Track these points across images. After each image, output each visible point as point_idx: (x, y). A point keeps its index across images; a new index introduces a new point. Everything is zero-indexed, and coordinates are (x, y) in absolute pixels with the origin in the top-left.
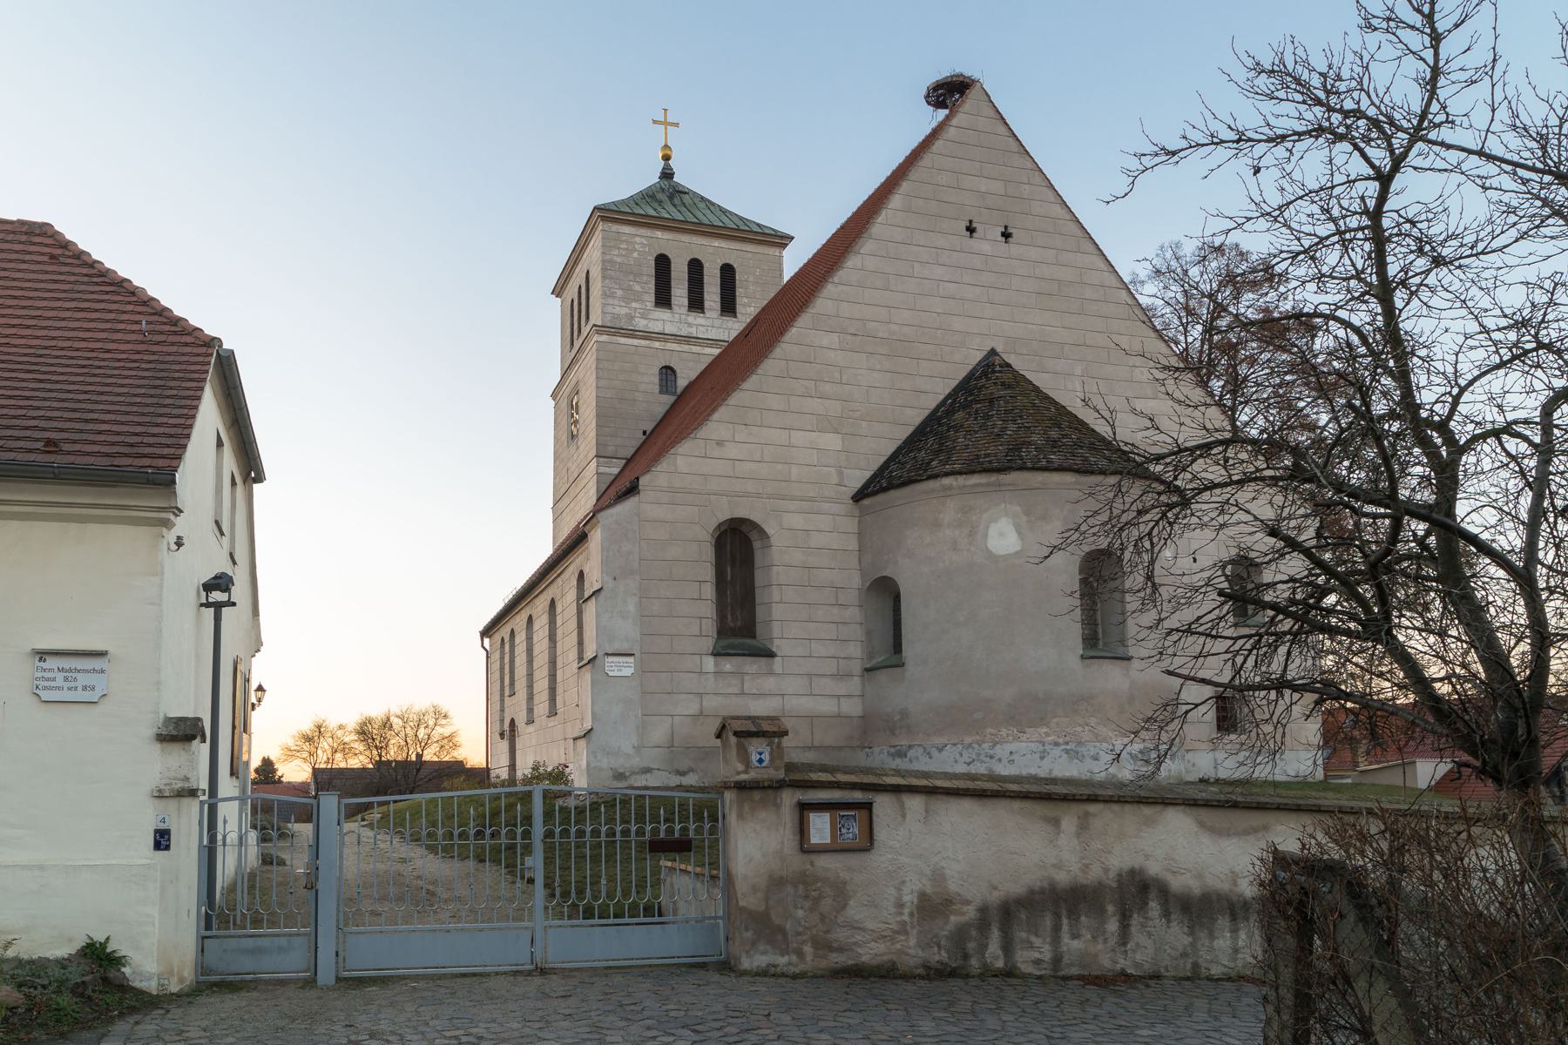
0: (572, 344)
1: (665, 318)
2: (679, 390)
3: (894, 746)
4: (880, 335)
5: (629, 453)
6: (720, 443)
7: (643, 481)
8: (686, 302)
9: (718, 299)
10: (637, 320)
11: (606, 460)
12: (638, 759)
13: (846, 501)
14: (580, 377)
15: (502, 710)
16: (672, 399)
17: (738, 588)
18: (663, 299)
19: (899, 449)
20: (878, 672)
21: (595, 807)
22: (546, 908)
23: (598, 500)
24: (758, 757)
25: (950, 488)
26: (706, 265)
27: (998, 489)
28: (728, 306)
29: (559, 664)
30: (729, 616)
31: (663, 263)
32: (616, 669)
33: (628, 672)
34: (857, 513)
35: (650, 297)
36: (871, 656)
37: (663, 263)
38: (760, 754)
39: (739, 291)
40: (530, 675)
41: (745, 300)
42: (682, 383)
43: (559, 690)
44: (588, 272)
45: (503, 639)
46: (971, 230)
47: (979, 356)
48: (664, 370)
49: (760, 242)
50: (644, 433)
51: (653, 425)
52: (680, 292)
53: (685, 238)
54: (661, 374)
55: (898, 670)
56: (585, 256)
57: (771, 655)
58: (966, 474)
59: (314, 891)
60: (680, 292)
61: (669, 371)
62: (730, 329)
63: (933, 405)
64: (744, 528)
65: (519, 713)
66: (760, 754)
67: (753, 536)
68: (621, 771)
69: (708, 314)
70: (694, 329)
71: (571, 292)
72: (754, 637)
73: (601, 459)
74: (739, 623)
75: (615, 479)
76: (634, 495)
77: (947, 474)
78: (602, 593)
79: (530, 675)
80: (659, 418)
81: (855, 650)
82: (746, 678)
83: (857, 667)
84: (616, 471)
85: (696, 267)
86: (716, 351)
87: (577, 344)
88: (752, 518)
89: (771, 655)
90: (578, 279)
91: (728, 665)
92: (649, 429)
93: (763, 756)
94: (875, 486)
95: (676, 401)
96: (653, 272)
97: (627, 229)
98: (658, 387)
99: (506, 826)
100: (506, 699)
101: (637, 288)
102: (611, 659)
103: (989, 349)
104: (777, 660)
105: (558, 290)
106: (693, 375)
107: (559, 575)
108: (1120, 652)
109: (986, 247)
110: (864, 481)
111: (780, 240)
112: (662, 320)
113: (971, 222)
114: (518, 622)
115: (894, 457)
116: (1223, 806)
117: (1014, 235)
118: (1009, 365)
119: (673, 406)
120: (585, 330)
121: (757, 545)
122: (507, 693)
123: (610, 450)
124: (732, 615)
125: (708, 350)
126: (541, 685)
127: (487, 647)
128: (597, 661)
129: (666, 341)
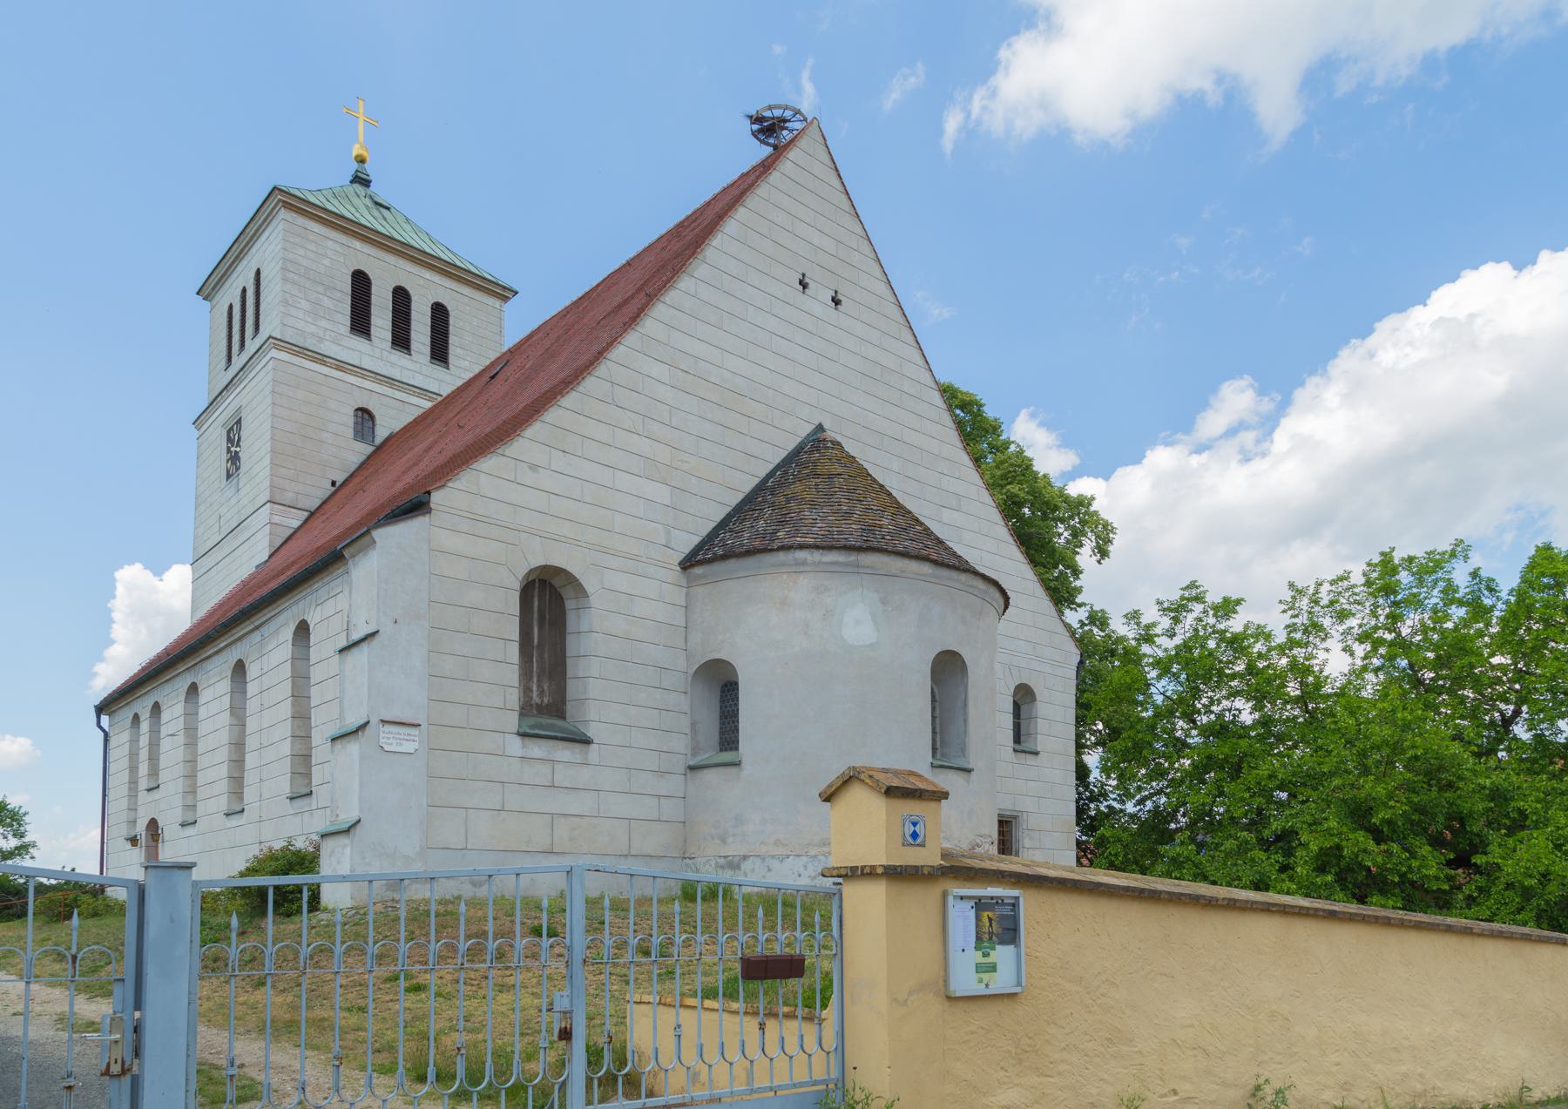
3: (725, 857)
4: (713, 380)
5: (314, 504)
6: (534, 467)
7: (437, 498)
8: (389, 336)
9: (428, 341)
10: (327, 343)
13: (673, 567)
14: (244, 403)
15: (133, 809)
16: (369, 449)
17: (546, 656)
18: (360, 323)
19: (728, 518)
20: (706, 771)
21: (388, 920)
22: (589, 1081)
23: (270, 557)
24: (912, 828)
25: (804, 563)
26: (414, 298)
27: (856, 570)
28: (440, 352)
29: (251, 743)
30: (535, 688)
31: (361, 283)
32: (394, 742)
33: (409, 747)
34: (684, 583)
35: (345, 319)
36: (695, 750)
37: (361, 283)
38: (915, 824)
39: (453, 340)
40: (192, 762)
42: (382, 433)
43: (250, 778)
44: (258, 273)
45: (136, 718)
46: (804, 285)
47: (809, 428)
48: (360, 413)
49: (479, 288)
50: (333, 483)
51: (346, 475)
52: (382, 319)
54: (356, 416)
55: (733, 770)
56: (253, 250)
57: (586, 741)
58: (823, 548)
59: (127, 1080)
60: (382, 319)
61: (366, 416)
62: (445, 382)
63: (763, 474)
64: (557, 582)
65: (166, 806)
66: (915, 824)
67: (567, 593)
71: (229, 295)
72: (564, 718)
73: (276, 506)
74: (546, 700)
76: (424, 514)
77: (801, 547)
78: (377, 639)
79: (192, 762)
80: (353, 469)
81: (680, 744)
83: (680, 764)
84: (296, 524)
85: (401, 298)
86: (428, 405)
87: (238, 362)
88: (569, 569)
89: (586, 741)
90: (242, 277)
91: (538, 749)
92: (340, 479)
93: (917, 829)
94: (704, 554)
96: (349, 289)
98: (352, 430)
99: (468, 937)
100: (143, 797)
101: (327, 302)
102: (388, 728)
103: (817, 423)
104: (593, 746)
105: (206, 291)
106: (397, 426)
107: (257, 628)
108: (962, 763)
109: (818, 309)
110: (692, 547)
111: (503, 293)
112: (354, 349)
113: (804, 275)
114: (171, 697)
115: (723, 524)
116: (1269, 910)
117: (843, 302)
118: (839, 444)
119: (369, 457)
120: (252, 346)
121: (570, 604)
122: (143, 784)
123: (288, 497)
125: (414, 400)
126: (215, 772)
129: (364, 377)
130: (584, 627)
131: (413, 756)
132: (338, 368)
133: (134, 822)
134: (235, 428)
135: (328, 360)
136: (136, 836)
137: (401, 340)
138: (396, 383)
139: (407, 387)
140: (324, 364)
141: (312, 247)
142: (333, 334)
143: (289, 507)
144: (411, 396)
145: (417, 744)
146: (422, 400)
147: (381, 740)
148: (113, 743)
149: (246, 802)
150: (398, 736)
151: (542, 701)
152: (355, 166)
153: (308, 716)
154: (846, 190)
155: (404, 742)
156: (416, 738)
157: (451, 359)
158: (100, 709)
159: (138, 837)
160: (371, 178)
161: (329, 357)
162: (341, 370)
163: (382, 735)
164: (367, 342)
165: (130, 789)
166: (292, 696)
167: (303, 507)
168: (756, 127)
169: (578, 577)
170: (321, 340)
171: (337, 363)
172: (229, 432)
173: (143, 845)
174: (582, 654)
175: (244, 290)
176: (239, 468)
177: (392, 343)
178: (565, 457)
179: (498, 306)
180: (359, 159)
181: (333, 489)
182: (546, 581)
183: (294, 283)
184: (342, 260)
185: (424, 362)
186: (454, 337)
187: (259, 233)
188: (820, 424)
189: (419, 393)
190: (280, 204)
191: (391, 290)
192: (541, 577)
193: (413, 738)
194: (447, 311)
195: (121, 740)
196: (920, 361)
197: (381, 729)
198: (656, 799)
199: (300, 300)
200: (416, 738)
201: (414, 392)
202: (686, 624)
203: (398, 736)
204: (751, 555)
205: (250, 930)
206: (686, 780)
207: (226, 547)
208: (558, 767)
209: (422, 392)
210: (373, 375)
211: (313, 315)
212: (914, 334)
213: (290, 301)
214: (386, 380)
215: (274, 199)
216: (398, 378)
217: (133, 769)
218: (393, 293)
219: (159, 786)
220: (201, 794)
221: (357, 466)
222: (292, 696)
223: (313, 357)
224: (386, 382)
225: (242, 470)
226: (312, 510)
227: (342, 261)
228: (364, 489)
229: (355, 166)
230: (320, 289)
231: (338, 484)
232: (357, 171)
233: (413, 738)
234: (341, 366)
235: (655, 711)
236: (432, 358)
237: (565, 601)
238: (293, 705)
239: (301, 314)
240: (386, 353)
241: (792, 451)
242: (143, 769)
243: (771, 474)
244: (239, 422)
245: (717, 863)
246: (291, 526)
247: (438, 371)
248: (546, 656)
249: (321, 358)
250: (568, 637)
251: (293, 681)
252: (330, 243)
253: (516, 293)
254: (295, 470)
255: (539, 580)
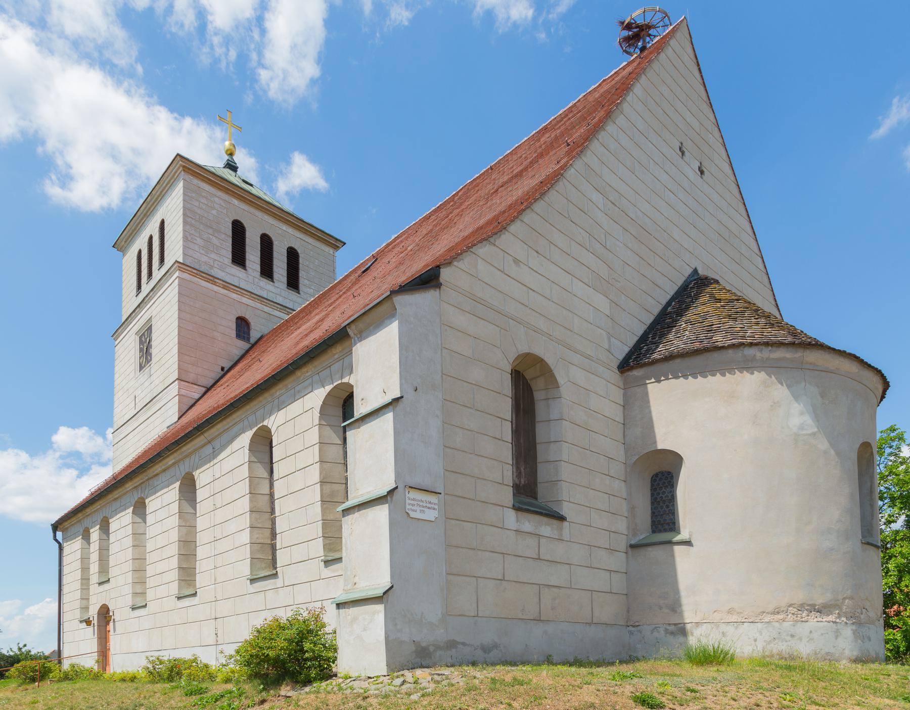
0: (139, 287)
1: (240, 276)
2: (253, 340)
3: (675, 624)
4: (630, 215)
6: (517, 261)
8: (258, 268)
9: (285, 273)
10: (215, 269)
11: (187, 384)
12: (442, 631)
14: (154, 314)
15: (85, 598)
16: (246, 346)
17: (522, 441)
18: (239, 258)
20: (650, 549)
23: (179, 419)
25: (753, 359)
28: (293, 282)
31: (238, 231)
32: (418, 509)
33: (431, 515)
36: (635, 535)
39: (302, 274)
41: (306, 281)
48: (240, 321)
49: (319, 239)
50: (223, 369)
53: (259, 214)
62: (297, 302)
68: (424, 644)
69: (276, 284)
70: (265, 292)
72: (536, 499)
73: (182, 383)
75: (196, 402)
78: (401, 405)
81: (622, 525)
82: (543, 541)
83: (623, 546)
84: (197, 396)
85: (266, 243)
86: (287, 317)
87: (146, 288)
88: (546, 359)
95: (251, 346)
97: (206, 187)
100: (94, 588)
101: (215, 241)
102: (414, 494)
103: (694, 268)
104: (566, 524)
111: (335, 243)
112: (235, 274)
120: (157, 274)
121: (538, 396)
122: (94, 579)
123: (191, 377)
124: (520, 471)
127: (60, 539)
128: (396, 495)
129: (242, 295)
130: (554, 415)
131: (434, 523)
132: (224, 288)
133: (85, 609)
134: (146, 333)
135: (217, 281)
136: (89, 618)
137: (267, 271)
138: (265, 301)
139: (272, 303)
140: (215, 284)
141: (203, 200)
142: (220, 263)
143: (192, 383)
144: (275, 311)
145: (437, 512)
146: (282, 314)
147: (408, 507)
148: (66, 551)
149: (198, 586)
150: (421, 504)
151: (520, 482)
152: (227, 157)
153: (254, 515)
154: (704, 82)
155: (426, 510)
156: (436, 507)
157: (301, 287)
158: (55, 527)
159: (91, 619)
160: (238, 165)
161: (218, 279)
162: (226, 289)
163: (408, 501)
164: (244, 271)
165: (82, 584)
166: (250, 493)
167: (201, 385)
168: (626, 33)
169: (552, 368)
170: (212, 267)
171: (224, 283)
172: (140, 338)
173: (96, 624)
174: (552, 440)
175: (151, 238)
176: (151, 360)
177: (261, 273)
178: (538, 257)
179: (331, 253)
180: (229, 152)
181: (222, 373)
182: (520, 372)
183: (192, 225)
184: (225, 211)
185: (283, 288)
186: (303, 272)
187: (163, 193)
188: (696, 269)
189: (280, 309)
190: (181, 168)
191: (260, 236)
192: (517, 369)
193: (433, 506)
194: (297, 253)
195: (68, 548)
196: (751, 232)
197: (407, 495)
198: (608, 574)
199: (196, 238)
200: (436, 507)
201: (277, 308)
202: (624, 422)
203: (421, 504)
204: (699, 354)
205: (270, 698)
206: (627, 558)
207: (141, 418)
208: (543, 541)
209: (282, 307)
210: (249, 294)
211: (205, 249)
212: (746, 209)
213: (189, 238)
214: (258, 298)
215: (177, 164)
216: (266, 297)
217: (85, 569)
218: (261, 238)
219: (109, 579)
220: (150, 583)
221: (239, 357)
222: (250, 493)
223: (206, 278)
224: (258, 300)
225: (154, 360)
226: (208, 387)
227: (225, 213)
228: (261, 360)
229: (227, 157)
230: (210, 231)
231: (226, 369)
232: (228, 160)
233: (433, 506)
234: (227, 285)
235: (605, 495)
236: (288, 285)
237: (534, 393)
238: (251, 501)
239: (197, 248)
240: (256, 280)
241: (681, 286)
242: (94, 568)
243: (669, 304)
244: (150, 329)
245: (666, 630)
246: (193, 397)
247: (292, 294)
248: (522, 441)
249: (212, 279)
250: (537, 425)
251: (250, 481)
252: (216, 199)
253: (345, 244)
254: (196, 358)
255: (515, 370)
